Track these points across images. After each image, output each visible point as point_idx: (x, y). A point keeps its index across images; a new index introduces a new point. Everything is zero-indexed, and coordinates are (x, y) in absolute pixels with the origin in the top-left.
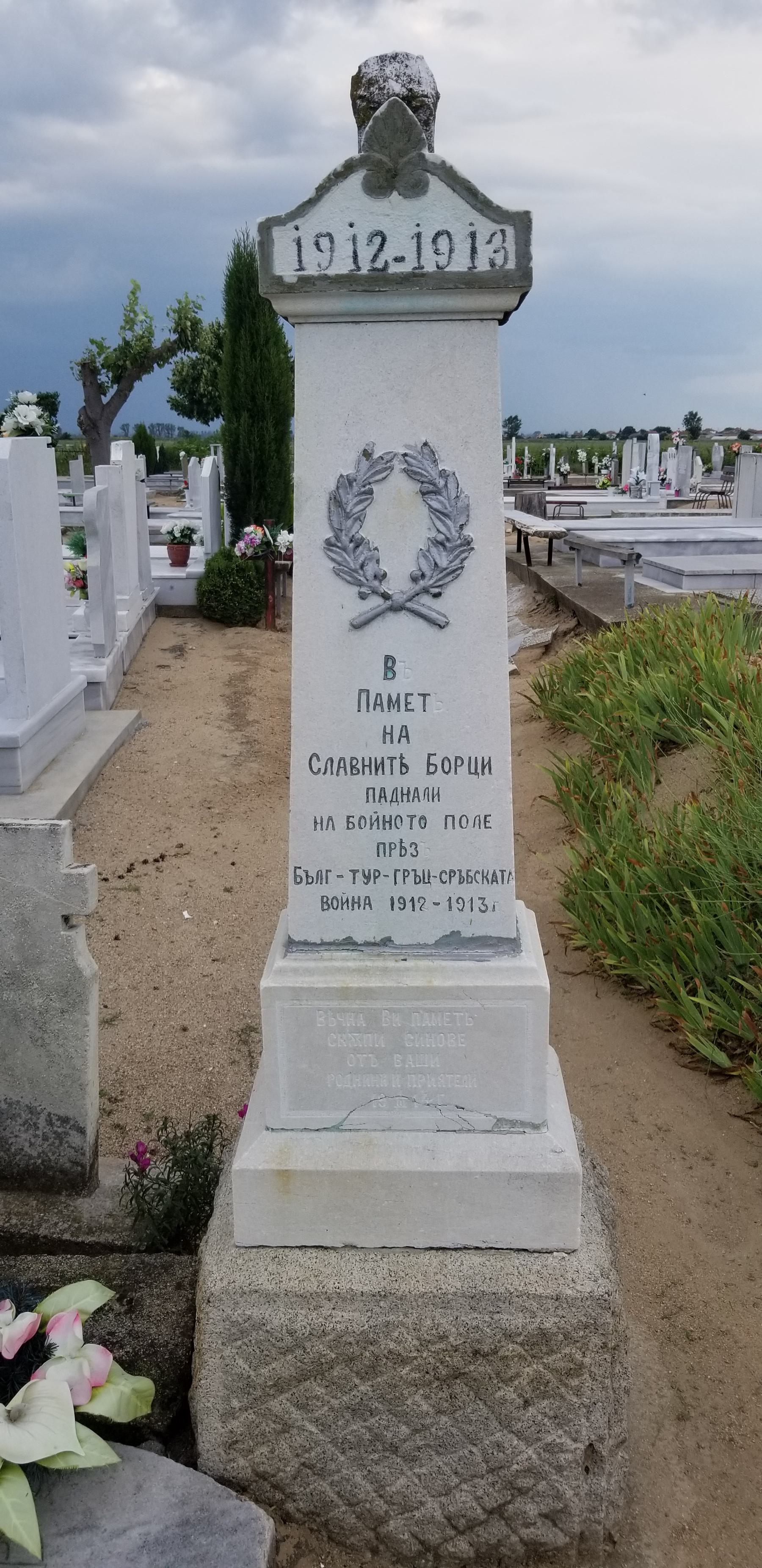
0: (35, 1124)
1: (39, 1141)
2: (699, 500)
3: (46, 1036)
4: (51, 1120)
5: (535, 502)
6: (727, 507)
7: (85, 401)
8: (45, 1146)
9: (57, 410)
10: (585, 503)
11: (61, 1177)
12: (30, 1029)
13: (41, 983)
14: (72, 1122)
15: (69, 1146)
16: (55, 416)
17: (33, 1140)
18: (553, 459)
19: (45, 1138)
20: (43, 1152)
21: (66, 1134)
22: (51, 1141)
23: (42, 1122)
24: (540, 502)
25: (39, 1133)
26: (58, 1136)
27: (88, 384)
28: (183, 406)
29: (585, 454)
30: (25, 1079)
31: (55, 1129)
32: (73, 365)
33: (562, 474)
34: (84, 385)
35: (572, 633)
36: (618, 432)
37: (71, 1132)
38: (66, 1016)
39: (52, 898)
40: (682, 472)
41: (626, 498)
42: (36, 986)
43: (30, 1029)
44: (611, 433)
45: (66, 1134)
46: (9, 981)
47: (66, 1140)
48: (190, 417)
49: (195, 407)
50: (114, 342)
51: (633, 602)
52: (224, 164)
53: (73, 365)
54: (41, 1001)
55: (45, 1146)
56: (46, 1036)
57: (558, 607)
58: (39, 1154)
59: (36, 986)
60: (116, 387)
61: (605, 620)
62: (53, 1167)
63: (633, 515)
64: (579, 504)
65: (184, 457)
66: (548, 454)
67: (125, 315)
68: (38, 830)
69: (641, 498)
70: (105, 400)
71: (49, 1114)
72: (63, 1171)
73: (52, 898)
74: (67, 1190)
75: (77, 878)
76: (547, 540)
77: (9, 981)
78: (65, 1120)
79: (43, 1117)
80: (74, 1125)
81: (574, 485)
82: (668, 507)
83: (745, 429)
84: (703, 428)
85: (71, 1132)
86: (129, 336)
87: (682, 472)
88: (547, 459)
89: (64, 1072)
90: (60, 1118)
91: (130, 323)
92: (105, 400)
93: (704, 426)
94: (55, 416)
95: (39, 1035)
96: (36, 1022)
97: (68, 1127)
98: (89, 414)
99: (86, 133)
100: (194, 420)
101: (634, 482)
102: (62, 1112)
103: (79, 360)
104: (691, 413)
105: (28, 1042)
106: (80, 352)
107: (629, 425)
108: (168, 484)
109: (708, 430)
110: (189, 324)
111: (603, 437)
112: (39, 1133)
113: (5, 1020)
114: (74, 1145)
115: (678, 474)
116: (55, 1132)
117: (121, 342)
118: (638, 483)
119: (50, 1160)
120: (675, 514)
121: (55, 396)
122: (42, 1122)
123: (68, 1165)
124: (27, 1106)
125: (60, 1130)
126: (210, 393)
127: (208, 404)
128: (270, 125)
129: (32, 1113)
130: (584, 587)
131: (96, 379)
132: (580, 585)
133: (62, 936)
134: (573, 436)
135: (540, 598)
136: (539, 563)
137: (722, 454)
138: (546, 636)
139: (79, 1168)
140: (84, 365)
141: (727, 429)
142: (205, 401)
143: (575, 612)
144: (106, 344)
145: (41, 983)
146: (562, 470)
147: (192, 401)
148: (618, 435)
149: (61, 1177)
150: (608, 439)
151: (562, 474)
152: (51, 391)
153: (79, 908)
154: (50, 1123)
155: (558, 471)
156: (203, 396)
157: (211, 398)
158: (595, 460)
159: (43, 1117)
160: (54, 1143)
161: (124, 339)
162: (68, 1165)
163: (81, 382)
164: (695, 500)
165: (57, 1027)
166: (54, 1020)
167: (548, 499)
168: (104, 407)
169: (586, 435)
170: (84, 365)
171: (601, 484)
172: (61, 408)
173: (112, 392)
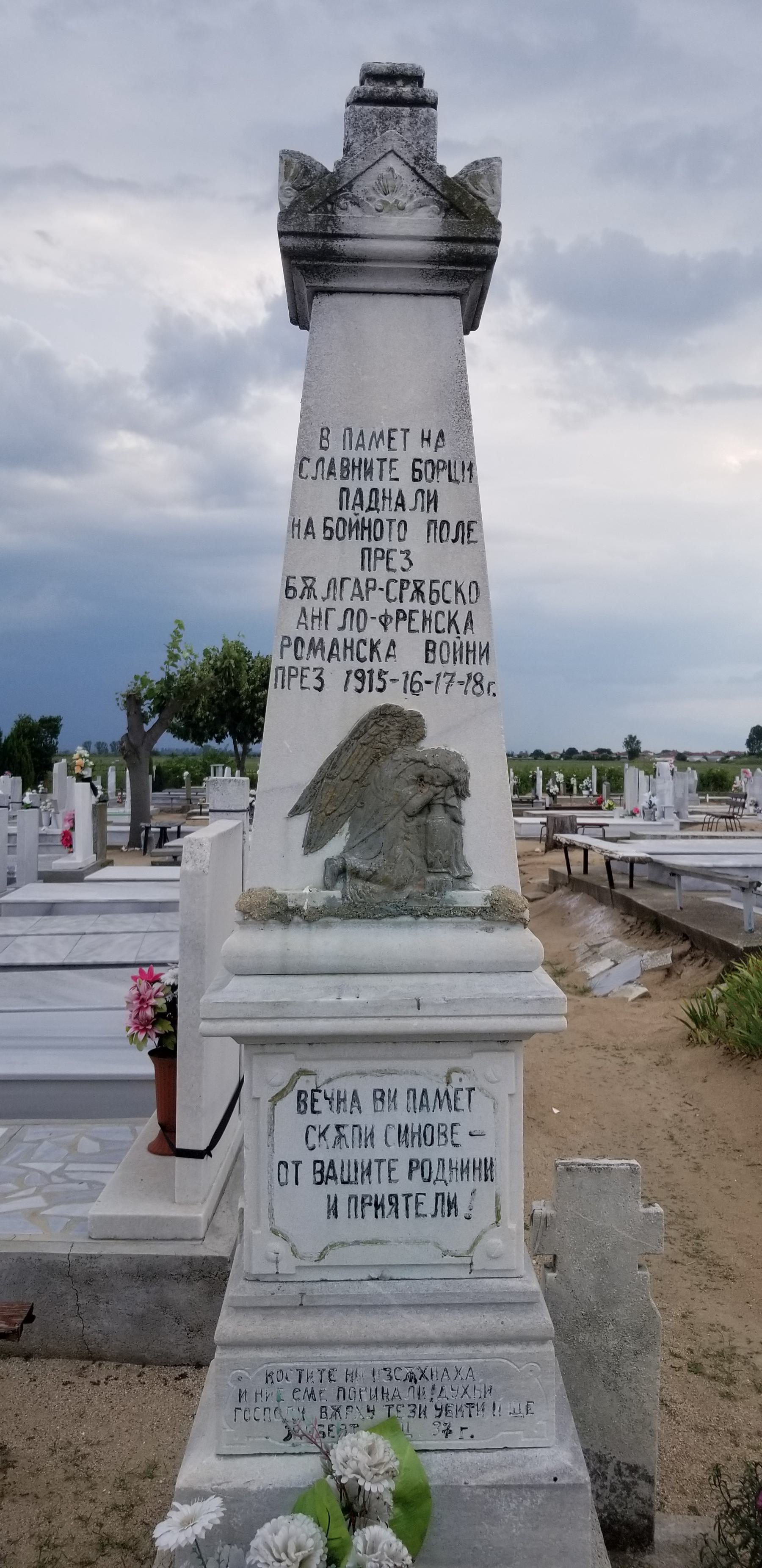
0: (603, 1474)
1: (607, 1492)
2: (709, 823)
3: (619, 1379)
4: (620, 1470)
5: (568, 824)
6: (732, 829)
7: (128, 728)
8: (612, 1498)
9: (58, 732)
10: (607, 825)
11: (627, 1531)
12: (604, 1372)
13: (616, 1324)
14: (641, 1471)
15: (638, 1498)
16: (56, 738)
17: (600, 1492)
18: (540, 781)
19: (613, 1490)
20: (610, 1504)
21: (635, 1483)
22: (618, 1492)
23: (610, 1472)
24: (572, 825)
25: (607, 1483)
26: (627, 1487)
27: (132, 713)
28: (179, 729)
29: (562, 776)
30: (596, 1426)
31: (624, 1479)
32: (118, 696)
33: (551, 795)
34: (128, 715)
35: (689, 956)
36: (561, 752)
37: (639, 1482)
38: (640, 1358)
39: (631, 1237)
40: (679, 795)
41: (638, 820)
42: (611, 1327)
43: (604, 1372)
44: (555, 753)
45: (635, 1483)
46: (586, 1323)
47: (633, 1490)
48: (185, 739)
49: (191, 730)
50: (157, 676)
51: (753, 927)
52: (186, 513)
53: (118, 696)
54: (615, 1342)
55: (612, 1498)
56: (619, 1379)
57: (659, 930)
58: (606, 1506)
59: (611, 1327)
60: (157, 716)
61: (735, 945)
62: (619, 1521)
63: (655, 837)
64: (601, 826)
65: (188, 776)
66: (535, 776)
67: (169, 652)
68: (620, 1170)
69: (655, 820)
70: (147, 728)
71: (618, 1463)
72: (629, 1525)
73: (631, 1237)
74: (631, 1546)
75: (655, 1217)
76: (628, 864)
77: (586, 1323)
78: (634, 1469)
79: (612, 1466)
80: (643, 1475)
81: (563, 805)
82: (681, 829)
83: (681, 751)
84: (642, 750)
85: (639, 1482)
86: (173, 670)
87: (679, 795)
88: (534, 780)
89: (635, 1417)
90: (629, 1467)
91: (174, 658)
92: (147, 728)
93: (643, 748)
94: (56, 738)
95: (612, 1378)
96: (609, 1365)
97: (636, 1476)
98: (131, 740)
99: (58, 484)
100: (189, 742)
101: (647, 806)
102: (630, 1460)
103: (124, 692)
104: (630, 737)
105: (601, 1386)
106: (125, 686)
107: (572, 747)
108: (169, 801)
109: (647, 752)
110: (232, 662)
111: (548, 757)
112: (607, 1483)
113: (579, 1363)
114: (641, 1496)
115: (675, 798)
116: (624, 1483)
117: (164, 676)
118: (650, 808)
119: (617, 1513)
120: (686, 837)
121: (58, 720)
122: (610, 1472)
123: (635, 1518)
124: (596, 1454)
125: (628, 1480)
126: (207, 717)
127: (204, 727)
128: (230, 482)
129: (600, 1461)
130: (685, 911)
131: (140, 710)
132: (681, 908)
133: (638, 1276)
134: (520, 756)
135: (631, 920)
136: (623, 886)
137: (696, 778)
138: (666, 958)
139: (646, 1521)
140: (129, 697)
141: (664, 751)
142: (201, 724)
143: (686, 935)
144: (150, 677)
145: (616, 1324)
146: (551, 791)
147: (188, 725)
148: (562, 756)
149: (627, 1531)
150: (553, 759)
151: (551, 795)
152: (55, 715)
153: (655, 1247)
154: (619, 1473)
155: (546, 791)
156: (200, 720)
157: (208, 721)
158: (573, 781)
159: (612, 1466)
160: (622, 1494)
161: (167, 674)
162: (635, 1518)
163: (125, 712)
164: (704, 823)
165: (629, 1370)
166: (628, 1363)
167: (579, 821)
168: (146, 734)
169: (531, 755)
170: (129, 697)
171: (607, 806)
172: (62, 730)
173: (153, 721)
